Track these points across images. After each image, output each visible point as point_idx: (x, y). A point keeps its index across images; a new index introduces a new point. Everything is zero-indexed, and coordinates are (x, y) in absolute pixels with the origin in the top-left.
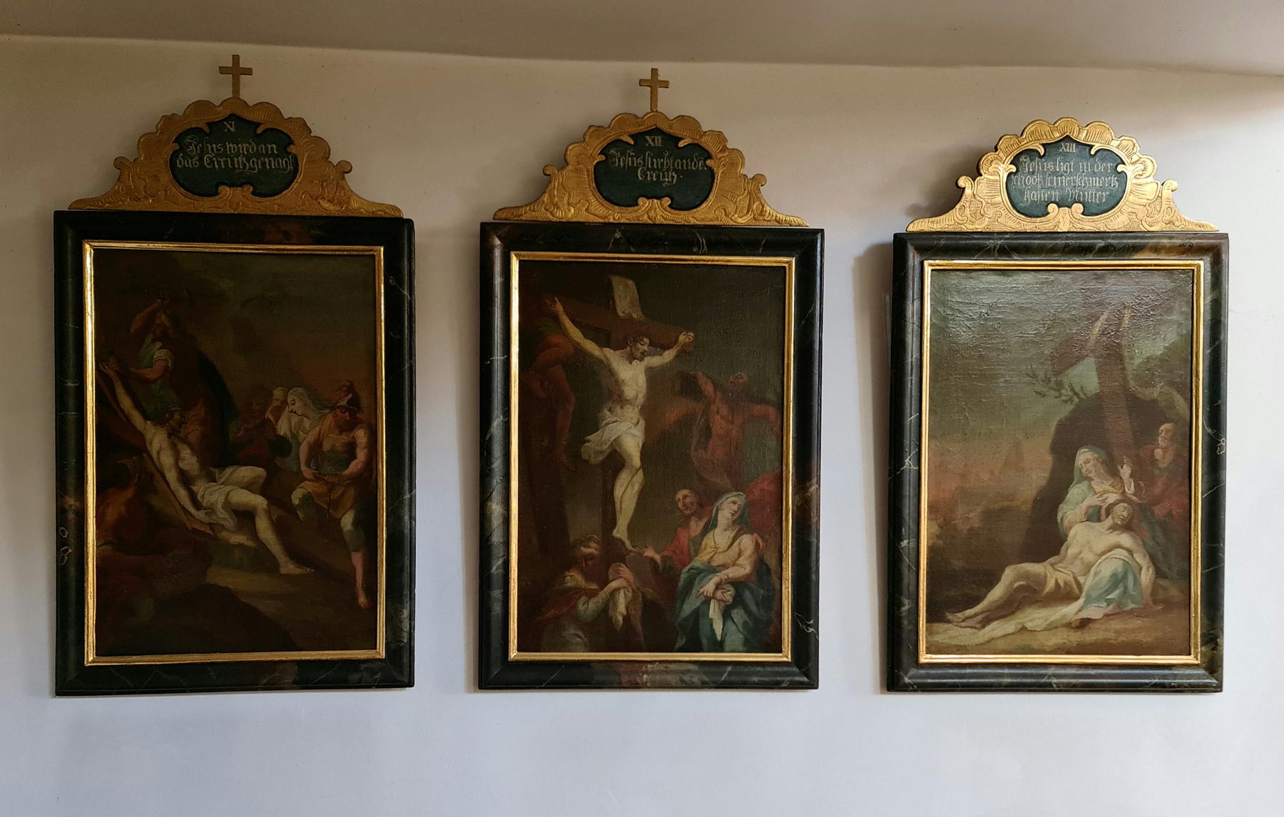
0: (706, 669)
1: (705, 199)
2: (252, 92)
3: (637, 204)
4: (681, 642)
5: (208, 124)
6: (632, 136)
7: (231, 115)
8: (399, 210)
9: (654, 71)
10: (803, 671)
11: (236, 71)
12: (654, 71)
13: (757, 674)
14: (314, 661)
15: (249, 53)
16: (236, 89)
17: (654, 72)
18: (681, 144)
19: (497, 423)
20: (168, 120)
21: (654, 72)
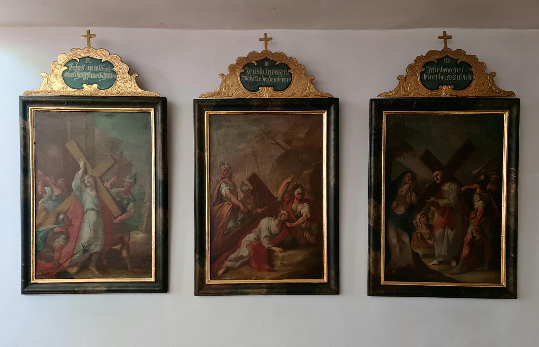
0: (104, 285)
1: (245, 87)
2: (453, 46)
3: (258, 90)
4: (74, 270)
5: (437, 60)
6: (256, 62)
7: (266, 58)
8: (513, 94)
9: (266, 34)
10: (162, 285)
11: (266, 39)
12: (266, 34)
13: (133, 287)
14: (247, 279)
15: (271, 33)
16: (446, 45)
17: (445, 32)
18: (276, 64)
19: (332, 183)
20: (419, 59)
21: (445, 32)
